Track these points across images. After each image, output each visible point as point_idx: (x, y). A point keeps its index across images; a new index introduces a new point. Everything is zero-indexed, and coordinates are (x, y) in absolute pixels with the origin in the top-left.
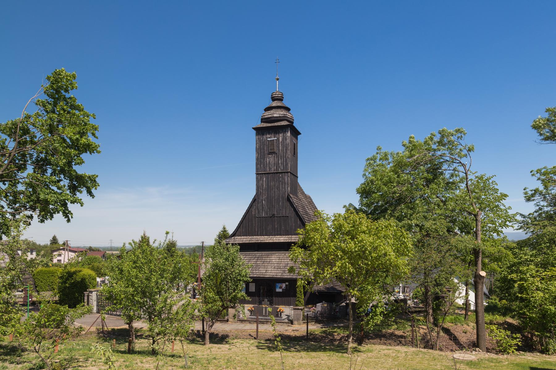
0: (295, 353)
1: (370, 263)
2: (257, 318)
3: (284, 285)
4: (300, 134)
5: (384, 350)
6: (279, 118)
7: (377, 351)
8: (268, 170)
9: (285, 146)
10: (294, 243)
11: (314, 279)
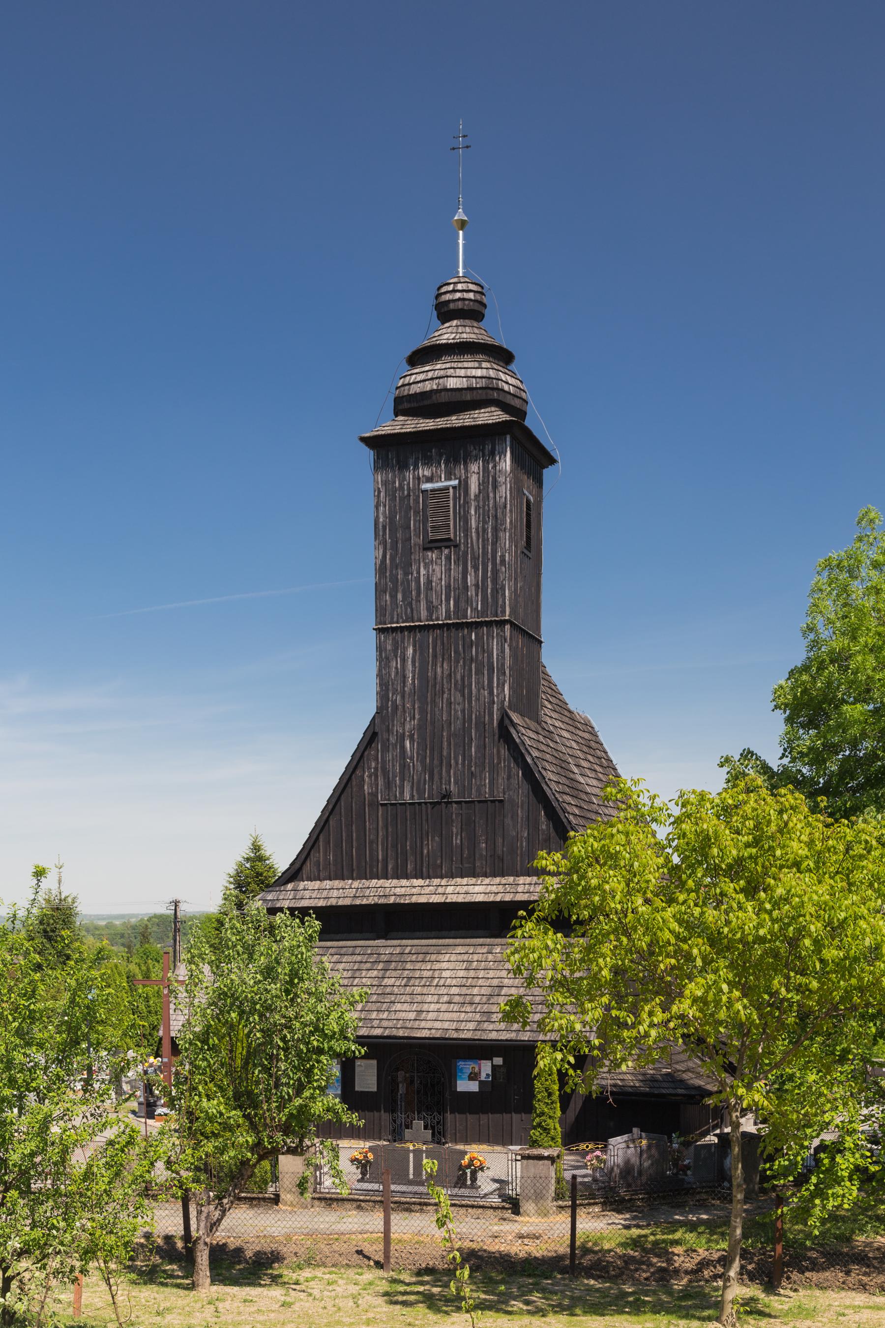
0: (526, 1319)
1: (815, 985)
2: (386, 1192)
3: (486, 1068)
4: (552, 461)
5: (857, 1309)
6: (468, 397)
7: (831, 1315)
8: (424, 614)
9: (492, 516)
10: (524, 905)
11: (601, 1048)
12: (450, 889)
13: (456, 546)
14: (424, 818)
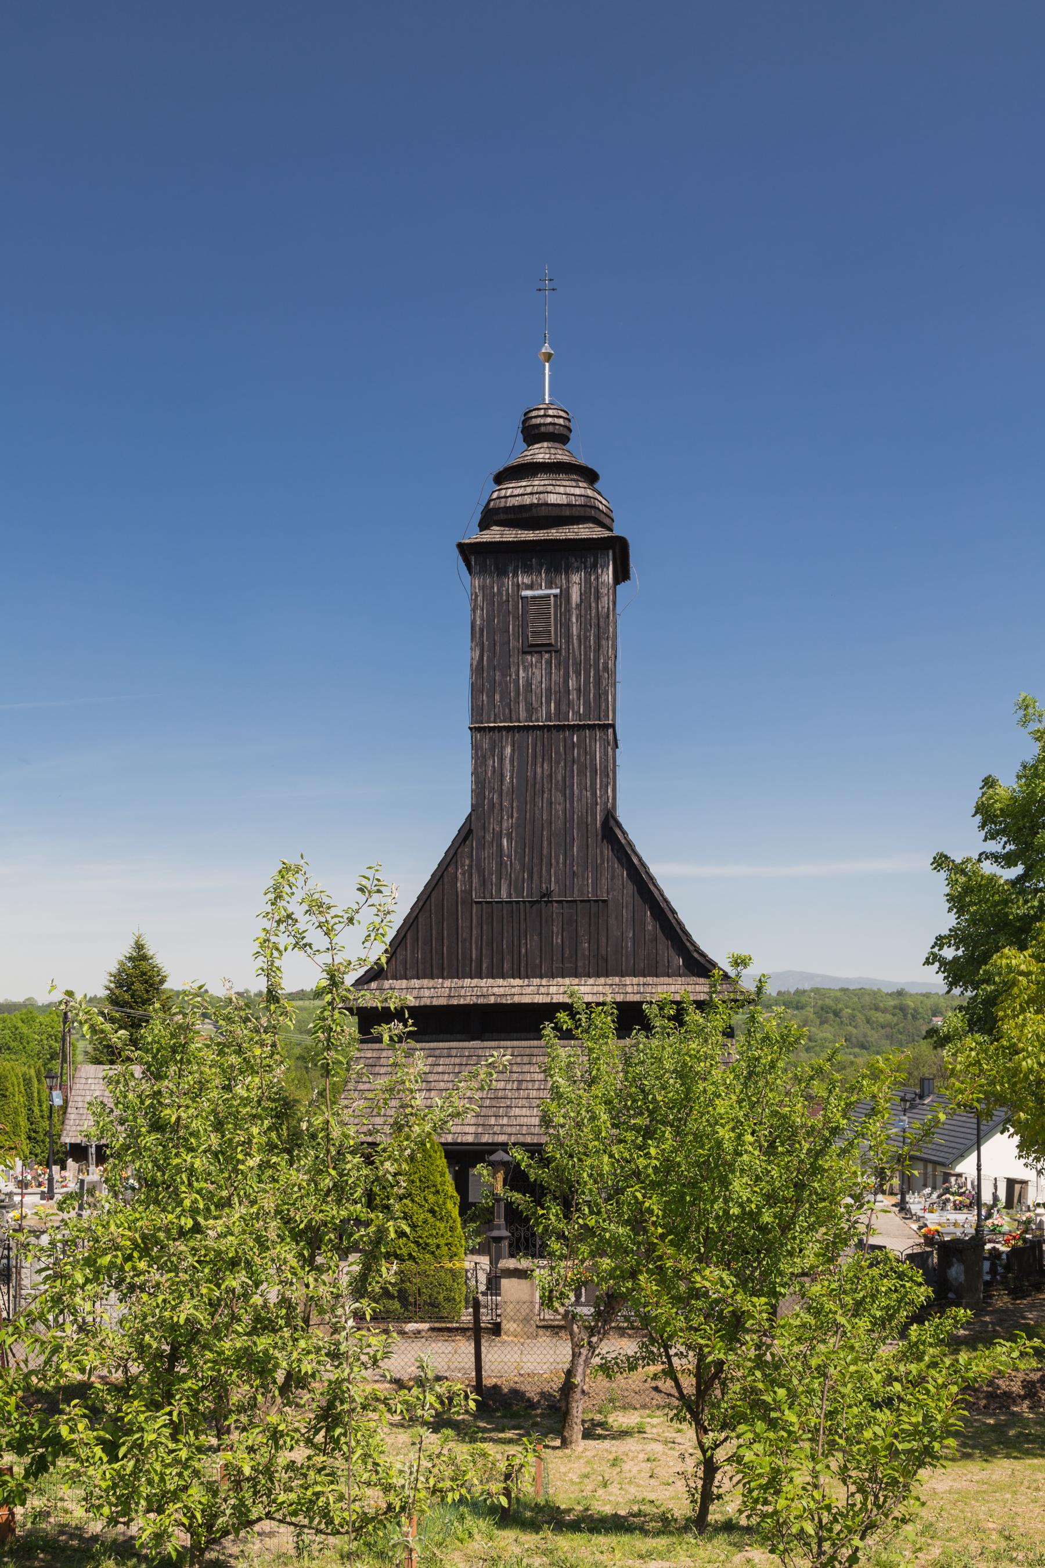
6: (567, 512)
8: (523, 714)
12: (553, 990)
13: (556, 652)
14: (522, 917)
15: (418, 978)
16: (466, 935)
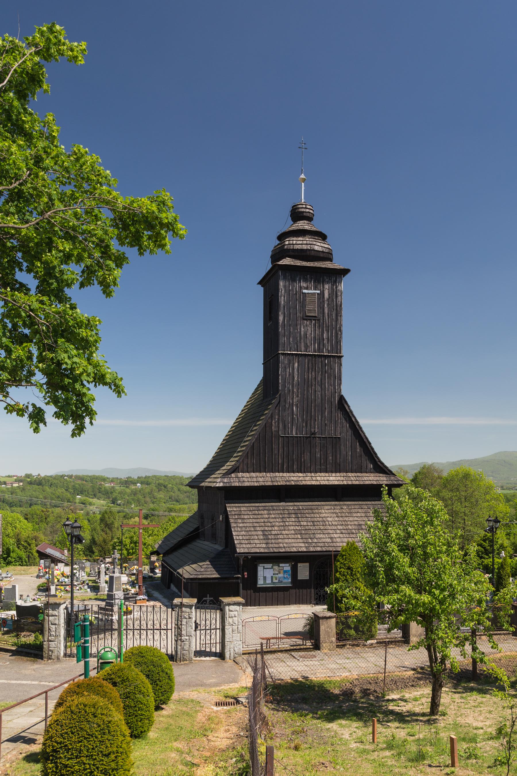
13: (318, 320)
14: (302, 444)
15: (254, 472)
16: (276, 452)
